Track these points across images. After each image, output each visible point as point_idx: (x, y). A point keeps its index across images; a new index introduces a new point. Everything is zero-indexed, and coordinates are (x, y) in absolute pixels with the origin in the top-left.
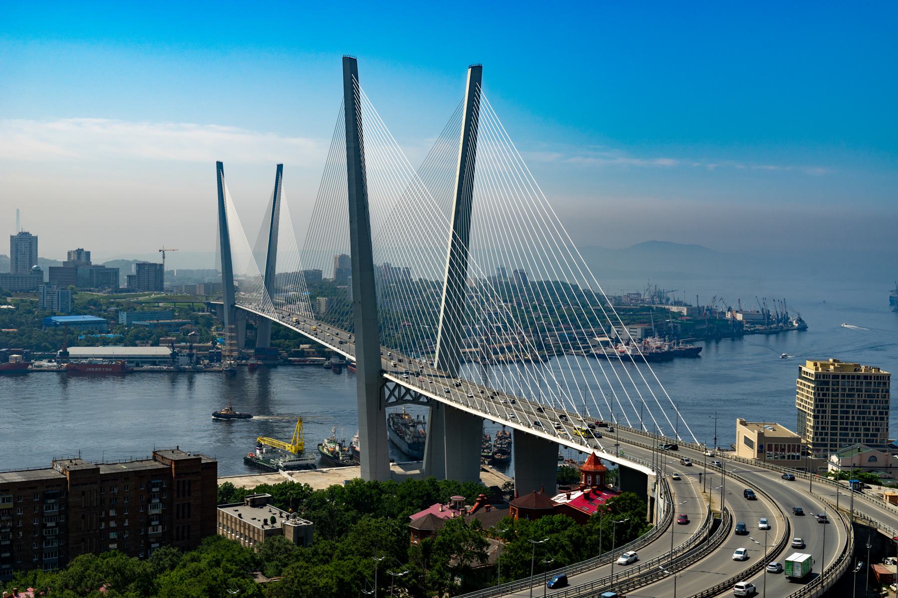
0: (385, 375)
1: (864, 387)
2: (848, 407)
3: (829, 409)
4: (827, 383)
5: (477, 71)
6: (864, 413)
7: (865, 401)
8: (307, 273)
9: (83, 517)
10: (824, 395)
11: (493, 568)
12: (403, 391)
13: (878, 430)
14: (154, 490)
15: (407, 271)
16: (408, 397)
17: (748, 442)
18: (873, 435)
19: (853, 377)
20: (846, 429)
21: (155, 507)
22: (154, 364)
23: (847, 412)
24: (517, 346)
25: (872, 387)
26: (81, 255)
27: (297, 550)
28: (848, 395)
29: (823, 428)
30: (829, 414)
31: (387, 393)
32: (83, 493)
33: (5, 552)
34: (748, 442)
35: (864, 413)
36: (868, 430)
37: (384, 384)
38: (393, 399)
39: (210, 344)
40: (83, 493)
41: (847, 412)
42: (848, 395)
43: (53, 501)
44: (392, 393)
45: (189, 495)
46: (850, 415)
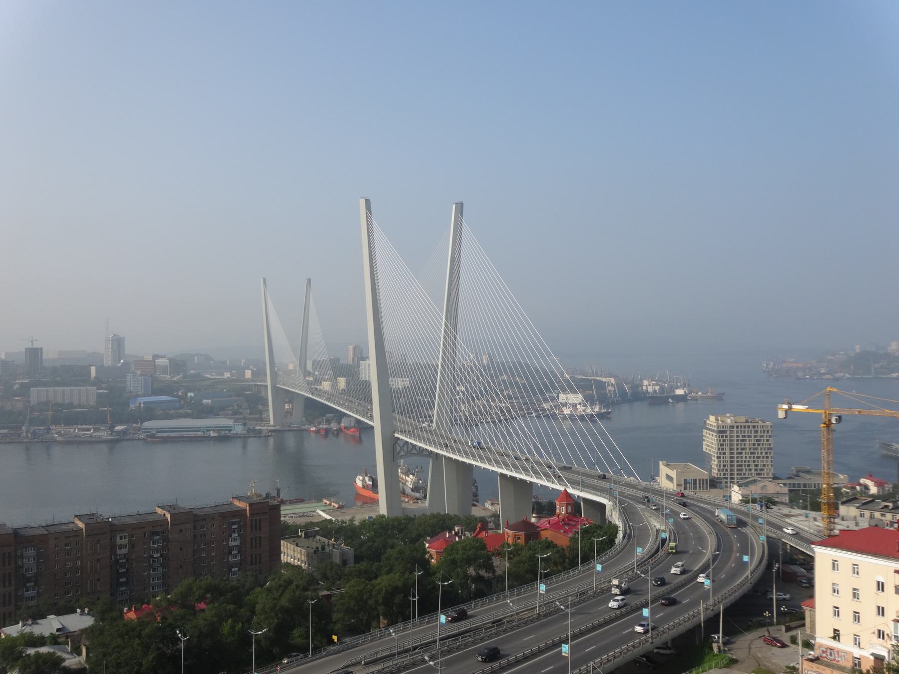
0: (396, 435)
1: (753, 434)
2: (742, 449)
3: (727, 451)
4: (725, 432)
5: (460, 207)
6: (754, 453)
7: (754, 445)
8: (331, 360)
9: (181, 549)
10: (724, 441)
11: (501, 579)
12: (410, 447)
13: (764, 466)
14: (234, 527)
16: (414, 451)
17: (669, 478)
18: (761, 470)
19: (745, 427)
20: (741, 466)
21: (235, 540)
22: (182, 437)
23: (741, 453)
24: (481, 412)
25: (759, 434)
26: (34, 354)
27: (670, 505)
28: (742, 441)
29: (724, 466)
30: (728, 455)
31: (398, 449)
32: (181, 531)
33: (122, 577)
34: (669, 478)
35: (754, 453)
36: (756, 466)
37: (396, 443)
39: (257, 416)
40: (181, 531)
41: (741, 453)
42: (742, 441)
43: (158, 537)
45: (260, 529)
46: (744, 455)
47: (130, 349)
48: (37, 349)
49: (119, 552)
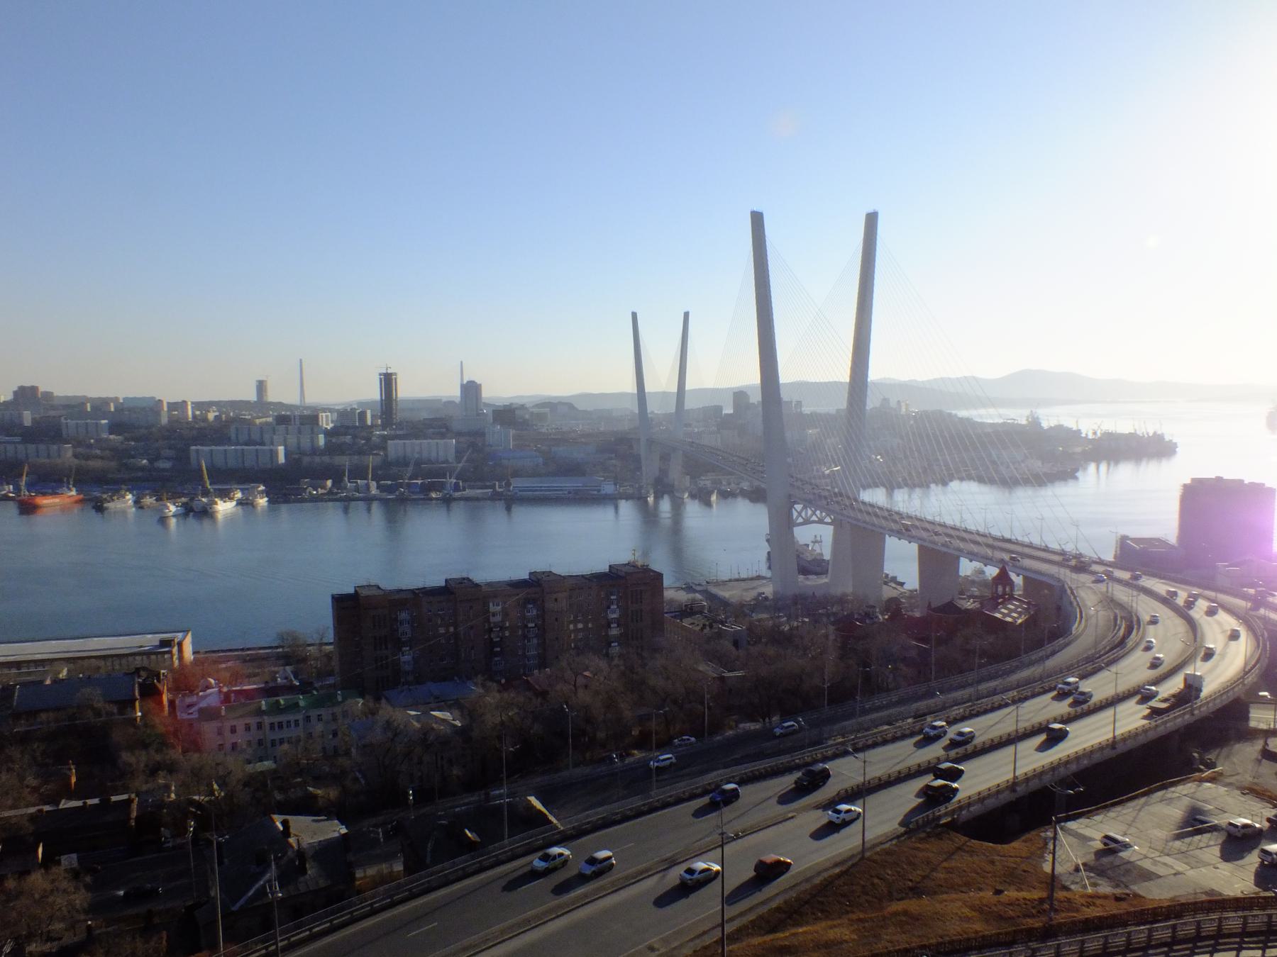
15: (799, 404)
16: (814, 518)
21: (614, 612)
31: (795, 514)
38: (800, 520)
44: (800, 514)
47: (404, 391)
48: (391, 375)
49: (492, 619)
